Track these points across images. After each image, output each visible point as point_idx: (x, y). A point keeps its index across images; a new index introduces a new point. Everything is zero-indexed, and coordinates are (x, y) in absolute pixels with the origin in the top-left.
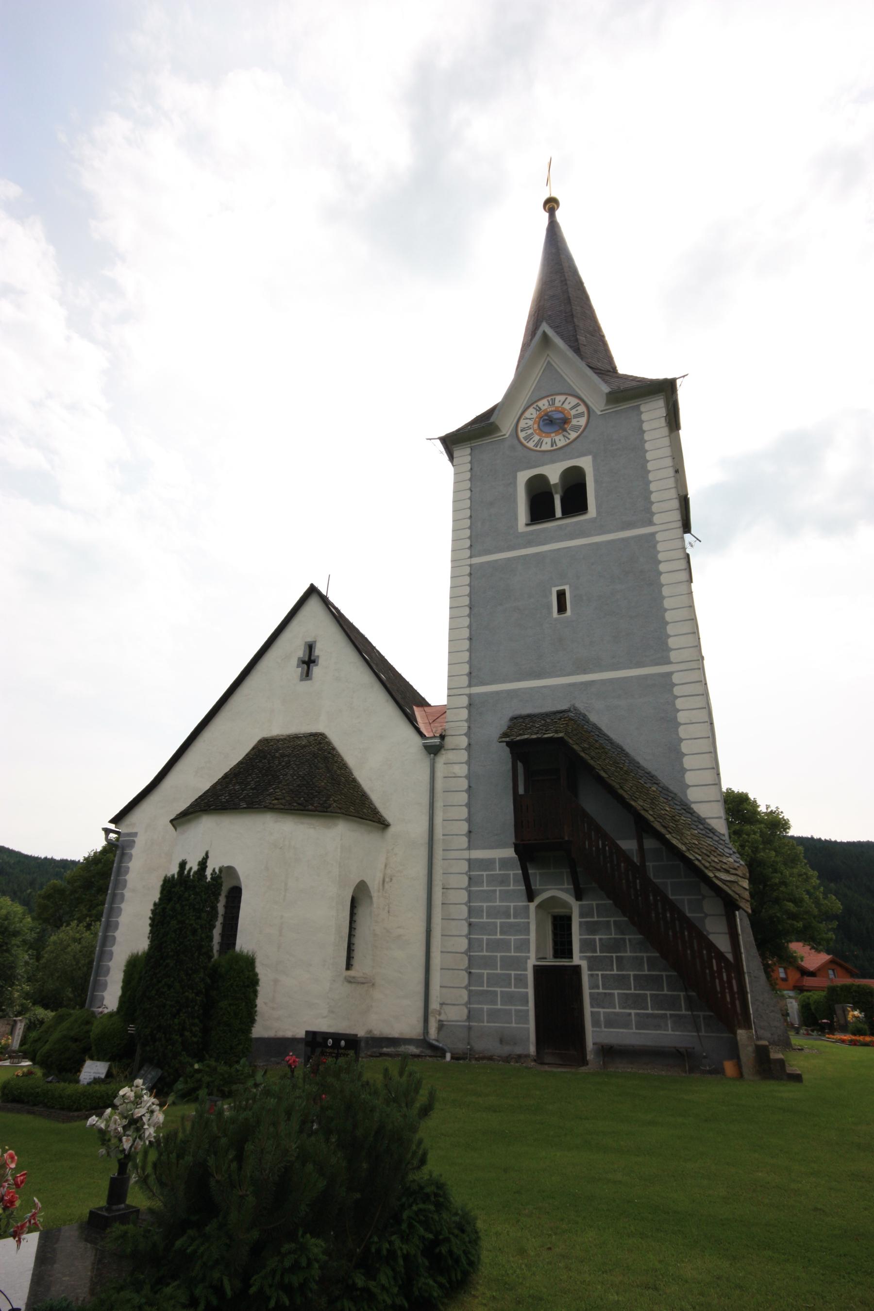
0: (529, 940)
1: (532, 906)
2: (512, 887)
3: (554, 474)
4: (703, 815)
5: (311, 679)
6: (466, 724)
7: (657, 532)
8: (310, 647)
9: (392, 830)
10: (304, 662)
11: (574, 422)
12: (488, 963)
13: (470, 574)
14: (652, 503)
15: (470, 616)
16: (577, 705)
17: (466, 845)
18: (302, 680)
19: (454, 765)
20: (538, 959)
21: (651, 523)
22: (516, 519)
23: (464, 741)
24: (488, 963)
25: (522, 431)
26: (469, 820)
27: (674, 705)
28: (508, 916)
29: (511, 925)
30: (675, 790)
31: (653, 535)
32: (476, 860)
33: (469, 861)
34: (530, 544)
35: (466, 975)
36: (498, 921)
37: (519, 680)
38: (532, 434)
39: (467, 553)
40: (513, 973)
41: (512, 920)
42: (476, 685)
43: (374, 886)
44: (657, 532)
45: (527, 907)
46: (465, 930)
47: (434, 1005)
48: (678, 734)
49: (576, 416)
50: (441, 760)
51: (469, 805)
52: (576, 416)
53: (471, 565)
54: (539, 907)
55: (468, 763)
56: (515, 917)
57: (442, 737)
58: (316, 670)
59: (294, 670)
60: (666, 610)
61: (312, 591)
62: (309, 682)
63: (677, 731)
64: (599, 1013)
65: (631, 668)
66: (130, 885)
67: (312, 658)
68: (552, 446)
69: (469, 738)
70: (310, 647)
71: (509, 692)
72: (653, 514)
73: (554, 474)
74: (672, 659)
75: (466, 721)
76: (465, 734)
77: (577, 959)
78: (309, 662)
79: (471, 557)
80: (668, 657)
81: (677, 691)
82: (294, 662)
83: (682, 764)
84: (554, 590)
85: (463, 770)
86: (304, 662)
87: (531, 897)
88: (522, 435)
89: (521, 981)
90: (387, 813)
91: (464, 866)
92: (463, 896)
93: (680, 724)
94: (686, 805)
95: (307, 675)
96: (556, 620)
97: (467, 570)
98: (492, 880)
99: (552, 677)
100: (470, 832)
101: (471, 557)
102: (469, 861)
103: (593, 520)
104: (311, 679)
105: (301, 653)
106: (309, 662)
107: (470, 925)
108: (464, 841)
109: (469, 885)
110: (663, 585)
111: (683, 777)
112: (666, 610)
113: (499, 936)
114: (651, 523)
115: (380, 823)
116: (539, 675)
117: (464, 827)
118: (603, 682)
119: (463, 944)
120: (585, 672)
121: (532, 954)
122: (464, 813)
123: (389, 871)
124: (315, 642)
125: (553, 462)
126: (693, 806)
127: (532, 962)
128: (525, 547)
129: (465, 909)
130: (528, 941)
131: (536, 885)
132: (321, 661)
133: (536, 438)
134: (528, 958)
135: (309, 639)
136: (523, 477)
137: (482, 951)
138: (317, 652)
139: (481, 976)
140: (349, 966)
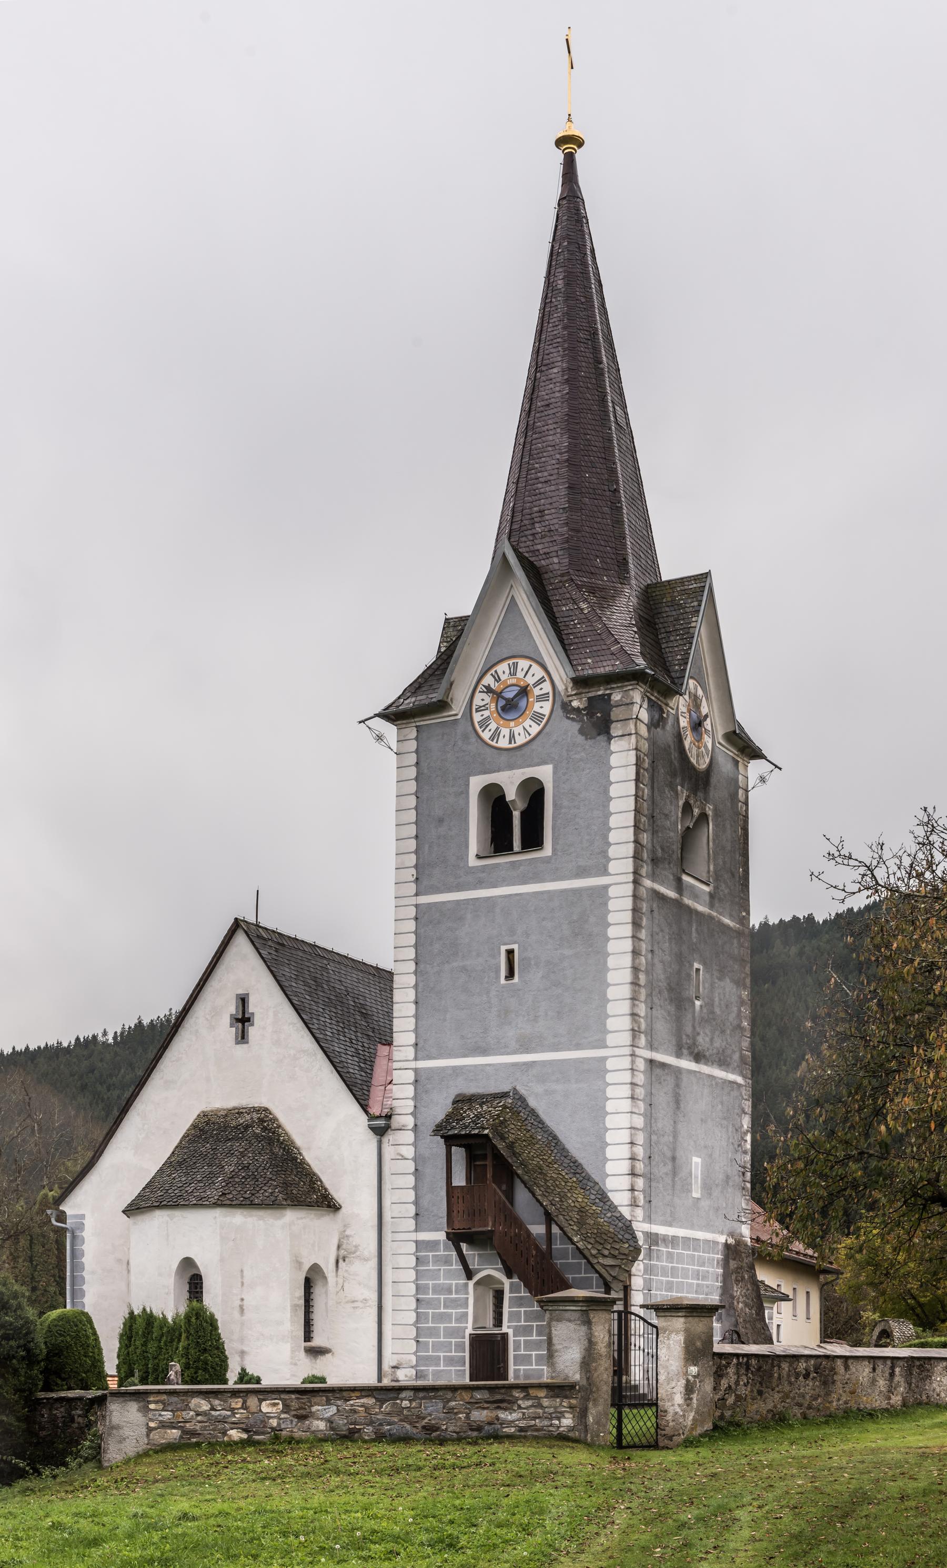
0: (467, 1313)
1: (471, 1284)
2: (454, 1267)
3: (510, 783)
4: (616, 1203)
5: (247, 1043)
6: (412, 1103)
7: (610, 885)
8: (243, 1001)
9: (343, 1210)
10: (238, 1020)
11: (537, 691)
12: (433, 1332)
13: (416, 919)
14: (609, 845)
15: (416, 973)
16: (518, 1088)
17: (413, 1228)
18: (237, 1043)
19: (402, 1143)
20: (474, 1329)
21: (605, 872)
22: (467, 847)
23: (410, 1121)
24: (433, 1332)
25: (477, 711)
26: (416, 1203)
27: (605, 1092)
28: (450, 1292)
29: (455, 1300)
30: (597, 1180)
31: (606, 887)
32: (423, 1241)
33: (416, 1242)
34: (480, 884)
35: (415, 1343)
36: (442, 1297)
37: (465, 1056)
38: (488, 718)
39: (412, 888)
40: (453, 1340)
41: (454, 1296)
42: (424, 1059)
43: (328, 1268)
44: (610, 885)
45: (466, 1285)
46: (414, 1306)
47: (386, 1367)
48: (604, 1123)
49: (536, 684)
50: (390, 1137)
51: (415, 1188)
52: (536, 684)
53: (416, 906)
54: (478, 1283)
55: (415, 1144)
56: (457, 1293)
57: (388, 1117)
58: (252, 1031)
59: (229, 1033)
60: (609, 985)
61: (237, 925)
62: (245, 1046)
63: (604, 1120)
64: (519, 1370)
65: (569, 1050)
66: (87, 1267)
67: (246, 1016)
68: (510, 743)
69: (415, 1118)
70: (243, 1001)
71: (454, 1069)
72: (609, 860)
73: (510, 783)
74: (608, 1044)
75: (412, 1099)
76: (411, 1114)
77: (505, 1329)
78: (243, 1020)
79: (417, 895)
80: (604, 1040)
81: (610, 1078)
82: (226, 1020)
83: (604, 1153)
84: (503, 949)
85: (409, 1152)
86: (238, 1020)
87: (469, 1274)
88: (477, 717)
89: (460, 1347)
90: (338, 1195)
91: (412, 1248)
92: (412, 1275)
93: (608, 1113)
94: (604, 1192)
95: (243, 1037)
96: (504, 986)
97: (412, 912)
98: (437, 1260)
99: (496, 1055)
100: (417, 1214)
101: (417, 895)
102: (416, 1242)
103: (547, 860)
104: (247, 1043)
105: (232, 1008)
106: (243, 1020)
107: (418, 1300)
108: (411, 1224)
109: (417, 1265)
110: (609, 955)
111: (604, 1166)
112: (609, 985)
113: (442, 1310)
114: (605, 872)
115: (327, 1203)
116: (484, 1052)
117: (412, 1210)
118: (544, 1063)
119: (412, 1317)
120: (527, 1051)
121: (470, 1325)
122: (411, 1196)
123: (342, 1252)
124: (248, 994)
125: (511, 767)
126: (609, 1194)
127: (469, 1330)
128: (475, 888)
129: (413, 1286)
130: (466, 1314)
131: (474, 1264)
132: (257, 1020)
133: (493, 726)
134: (466, 1328)
135: (240, 992)
136: (477, 783)
137: (428, 1323)
138: (251, 1008)
139: (427, 1343)
140: (308, 1337)
